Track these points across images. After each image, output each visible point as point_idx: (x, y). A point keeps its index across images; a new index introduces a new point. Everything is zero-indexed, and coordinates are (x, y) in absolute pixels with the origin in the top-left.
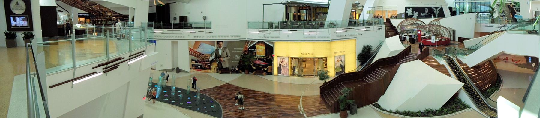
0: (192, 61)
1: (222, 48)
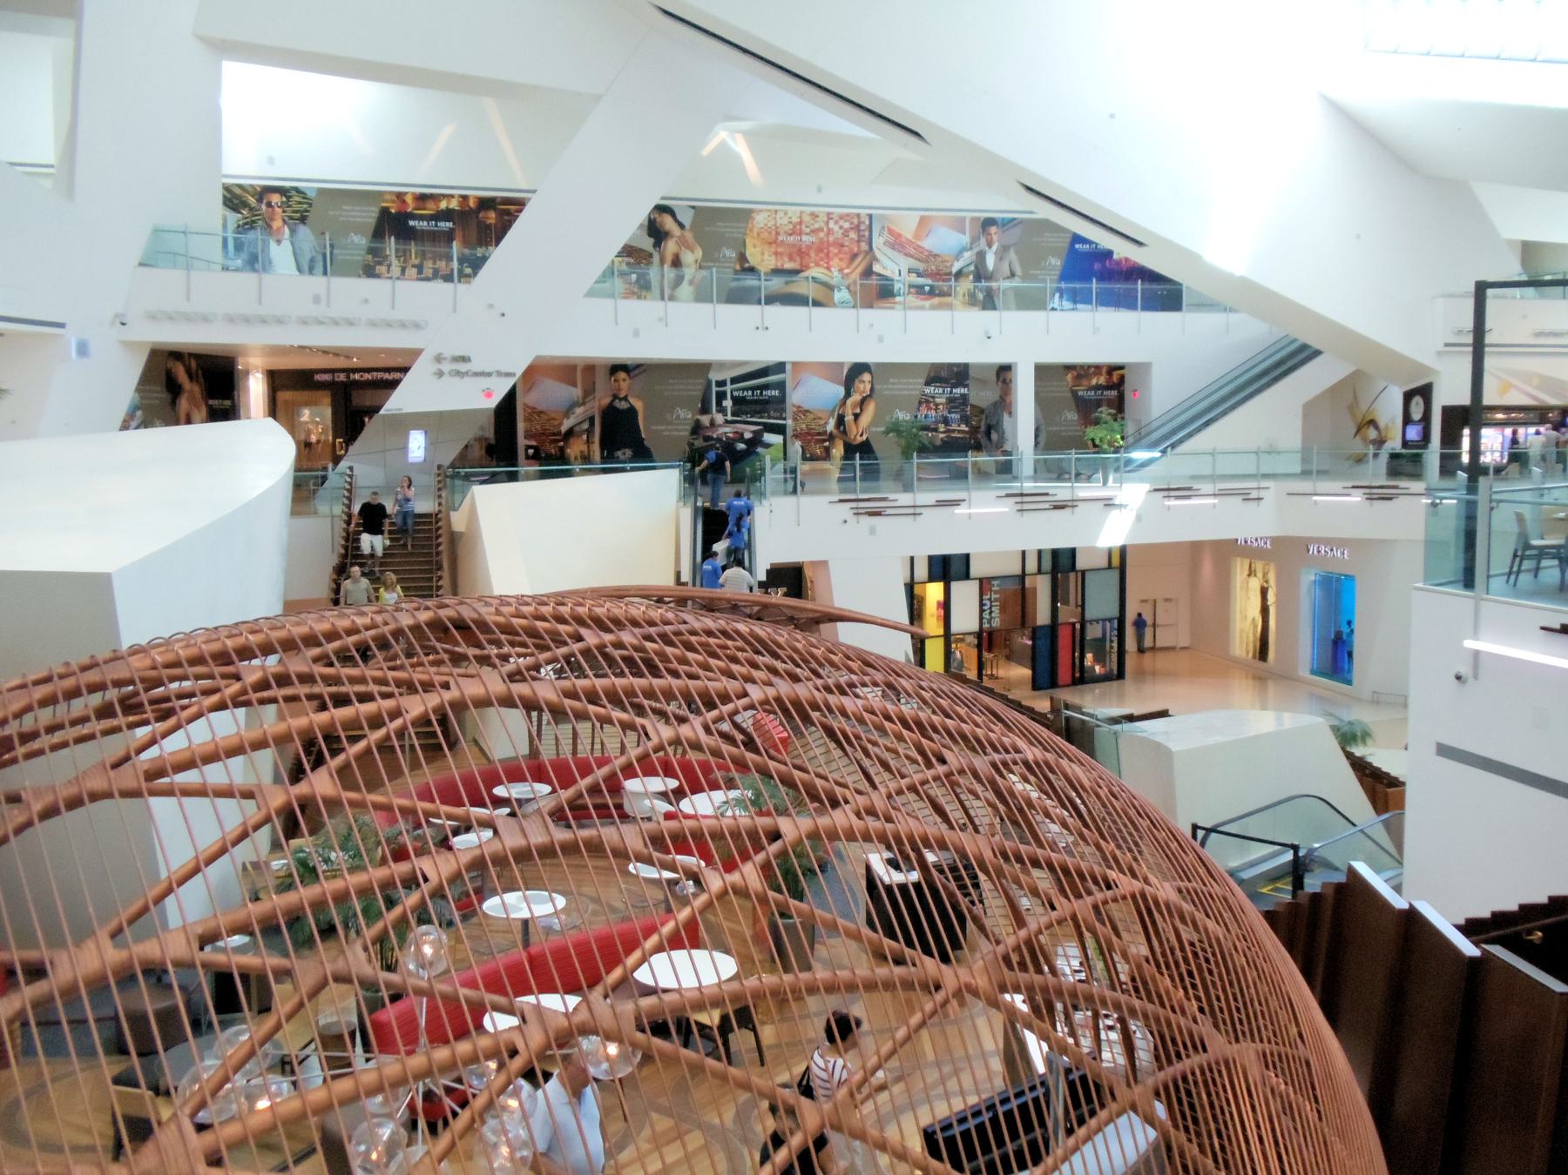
1: (995, 247)
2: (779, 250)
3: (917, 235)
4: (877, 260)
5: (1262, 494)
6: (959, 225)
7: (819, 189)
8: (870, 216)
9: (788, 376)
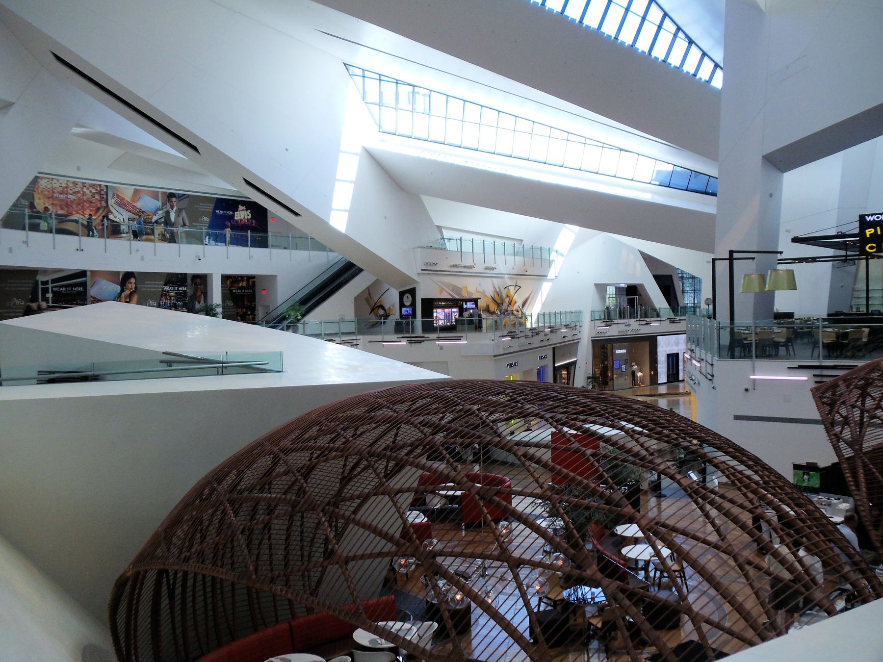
0: (129, 220)
1: (175, 209)
2: (55, 202)
3: (133, 200)
4: (111, 212)
5: (359, 342)
6: (155, 195)
7: (79, 169)
8: (107, 186)
9: (88, 279)
